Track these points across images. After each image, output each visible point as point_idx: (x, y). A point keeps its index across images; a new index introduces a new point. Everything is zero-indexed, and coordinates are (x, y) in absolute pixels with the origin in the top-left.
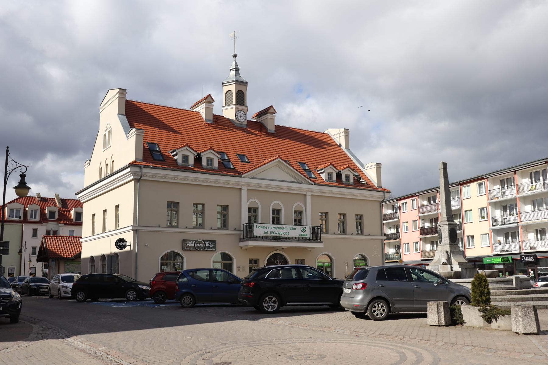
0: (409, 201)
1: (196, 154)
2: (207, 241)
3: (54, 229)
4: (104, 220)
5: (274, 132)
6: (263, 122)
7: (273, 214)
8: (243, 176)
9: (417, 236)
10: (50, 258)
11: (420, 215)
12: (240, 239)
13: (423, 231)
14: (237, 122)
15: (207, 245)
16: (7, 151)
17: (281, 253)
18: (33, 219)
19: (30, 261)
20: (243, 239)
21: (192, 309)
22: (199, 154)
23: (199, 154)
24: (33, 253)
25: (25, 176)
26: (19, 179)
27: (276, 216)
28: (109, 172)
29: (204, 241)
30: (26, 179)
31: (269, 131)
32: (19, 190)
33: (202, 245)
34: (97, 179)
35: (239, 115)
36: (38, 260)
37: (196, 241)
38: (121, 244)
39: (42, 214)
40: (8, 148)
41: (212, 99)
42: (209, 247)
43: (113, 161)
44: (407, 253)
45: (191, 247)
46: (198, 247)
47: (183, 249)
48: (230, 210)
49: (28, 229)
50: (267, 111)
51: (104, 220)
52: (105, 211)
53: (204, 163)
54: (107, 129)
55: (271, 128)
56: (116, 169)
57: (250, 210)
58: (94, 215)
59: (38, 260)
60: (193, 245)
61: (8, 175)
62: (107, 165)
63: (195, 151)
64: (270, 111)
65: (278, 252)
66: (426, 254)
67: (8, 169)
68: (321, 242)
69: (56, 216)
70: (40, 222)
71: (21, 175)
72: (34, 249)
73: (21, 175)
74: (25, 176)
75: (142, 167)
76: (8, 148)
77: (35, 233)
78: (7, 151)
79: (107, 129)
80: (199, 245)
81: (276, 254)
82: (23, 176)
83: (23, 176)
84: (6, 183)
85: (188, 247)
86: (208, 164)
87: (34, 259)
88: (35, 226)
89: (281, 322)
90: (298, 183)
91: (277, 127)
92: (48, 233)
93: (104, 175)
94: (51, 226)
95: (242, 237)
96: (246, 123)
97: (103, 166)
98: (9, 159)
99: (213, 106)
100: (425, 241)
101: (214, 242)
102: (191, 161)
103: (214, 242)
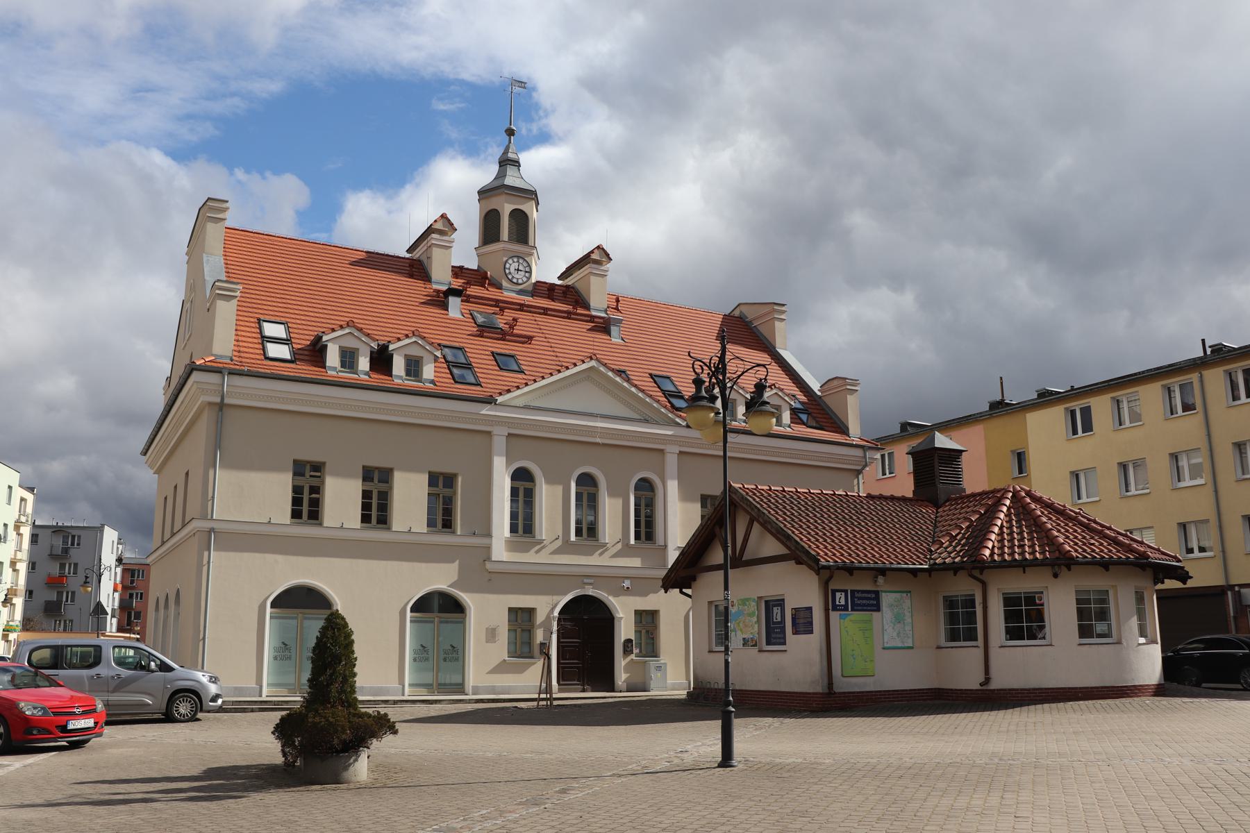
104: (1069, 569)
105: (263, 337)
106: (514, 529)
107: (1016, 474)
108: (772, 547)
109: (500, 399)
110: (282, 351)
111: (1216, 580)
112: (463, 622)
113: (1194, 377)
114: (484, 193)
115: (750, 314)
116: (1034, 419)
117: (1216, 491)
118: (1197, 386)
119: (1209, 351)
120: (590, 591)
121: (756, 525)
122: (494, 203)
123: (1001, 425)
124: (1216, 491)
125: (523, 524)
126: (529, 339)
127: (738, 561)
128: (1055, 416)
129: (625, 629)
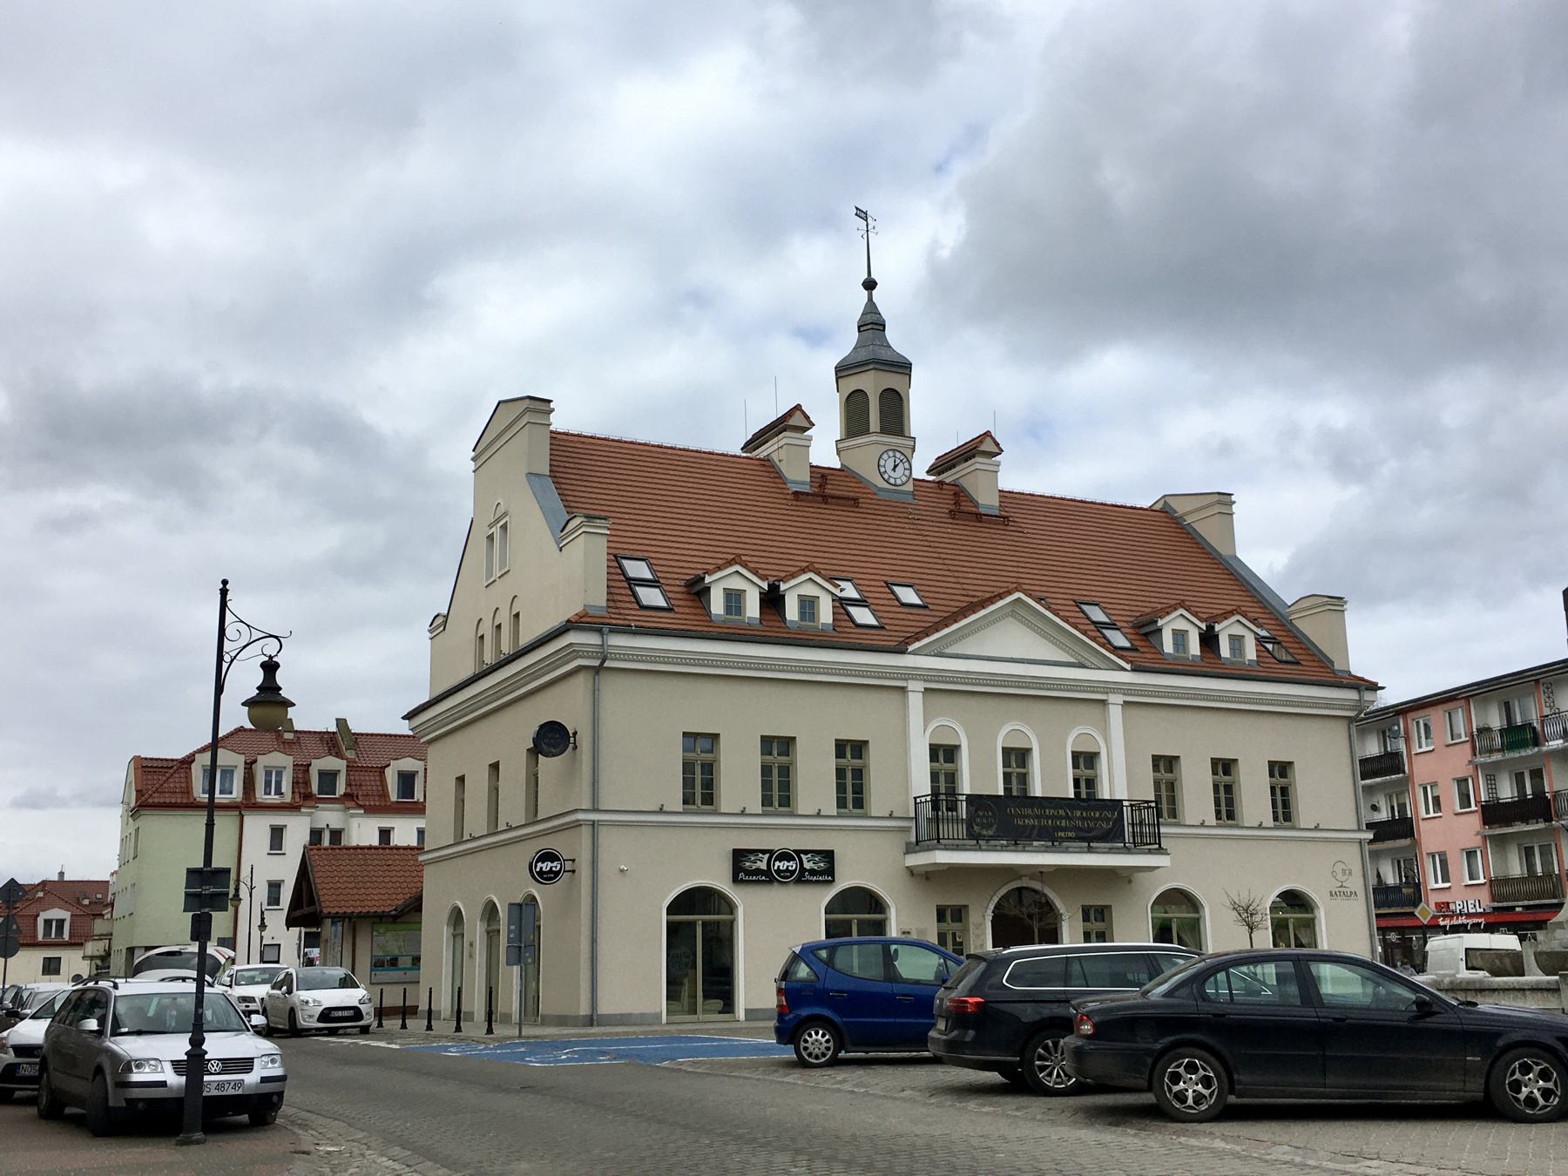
0: (1437, 716)
1: (765, 586)
2: (806, 852)
3: (335, 825)
4: (494, 792)
5: (997, 513)
6: (963, 482)
7: (1006, 764)
8: (911, 648)
9: (1465, 829)
10: (329, 916)
11: (1480, 759)
12: (908, 844)
13: (1493, 813)
14: (882, 484)
15: (807, 865)
16: (224, 592)
17: (1037, 886)
18: (273, 798)
19: (263, 926)
20: (917, 842)
21: (830, 1072)
22: (774, 588)
23: (774, 588)
24: (274, 899)
25: (277, 666)
26: (258, 677)
27: (1015, 770)
28: (506, 648)
29: (798, 852)
30: (280, 677)
31: (982, 511)
32: (259, 711)
33: (792, 865)
34: (468, 671)
35: (890, 464)
36: (290, 923)
37: (771, 852)
38: (546, 866)
39: (301, 782)
40: (225, 582)
41: (807, 418)
42: (812, 872)
43: (517, 616)
44: (1441, 885)
45: (758, 872)
46: (778, 871)
47: (736, 880)
48: (876, 761)
49: (257, 828)
50: (979, 449)
51: (494, 792)
52: (495, 767)
53: (792, 611)
54: (497, 521)
55: (797, 476)
56: (525, 639)
57: (935, 751)
58: (461, 780)
59: (290, 923)
60: (763, 866)
61: (225, 666)
62: (499, 627)
63: (763, 578)
64: (792, 422)
65: (1025, 883)
66: (1506, 890)
67: (227, 646)
68: (1161, 851)
69: (341, 788)
70: (292, 808)
71: (263, 665)
72: (275, 887)
73: (263, 665)
74: (277, 666)
75: (606, 630)
76: (225, 582)
77: (277, 834)
78: (224, 592)
79: (497, 521)
80: (783, 865)
81: (1020, 890)
82: (270, 667)
83: (270, 667)
84: (219, 689)
85: (749, 872)
86: (728, 610)
87: (277, 919)
88: (278, 819)
89: (1281, 1152)
90: (1082, 666)
91: (1005, 495)
92: (316, 834)
93: (489, 659)
94: (330, 817)
95: (913, 839)
96: (909, 487)
97: (487, 629)
98: (229, 617)
99: (810, 439)
100: (1500, 842)
101: (828, 856)
102: (752, 608)
103: (828, 856)
105: (629, 579)
115: (1180, 508)
122: (853, 383)
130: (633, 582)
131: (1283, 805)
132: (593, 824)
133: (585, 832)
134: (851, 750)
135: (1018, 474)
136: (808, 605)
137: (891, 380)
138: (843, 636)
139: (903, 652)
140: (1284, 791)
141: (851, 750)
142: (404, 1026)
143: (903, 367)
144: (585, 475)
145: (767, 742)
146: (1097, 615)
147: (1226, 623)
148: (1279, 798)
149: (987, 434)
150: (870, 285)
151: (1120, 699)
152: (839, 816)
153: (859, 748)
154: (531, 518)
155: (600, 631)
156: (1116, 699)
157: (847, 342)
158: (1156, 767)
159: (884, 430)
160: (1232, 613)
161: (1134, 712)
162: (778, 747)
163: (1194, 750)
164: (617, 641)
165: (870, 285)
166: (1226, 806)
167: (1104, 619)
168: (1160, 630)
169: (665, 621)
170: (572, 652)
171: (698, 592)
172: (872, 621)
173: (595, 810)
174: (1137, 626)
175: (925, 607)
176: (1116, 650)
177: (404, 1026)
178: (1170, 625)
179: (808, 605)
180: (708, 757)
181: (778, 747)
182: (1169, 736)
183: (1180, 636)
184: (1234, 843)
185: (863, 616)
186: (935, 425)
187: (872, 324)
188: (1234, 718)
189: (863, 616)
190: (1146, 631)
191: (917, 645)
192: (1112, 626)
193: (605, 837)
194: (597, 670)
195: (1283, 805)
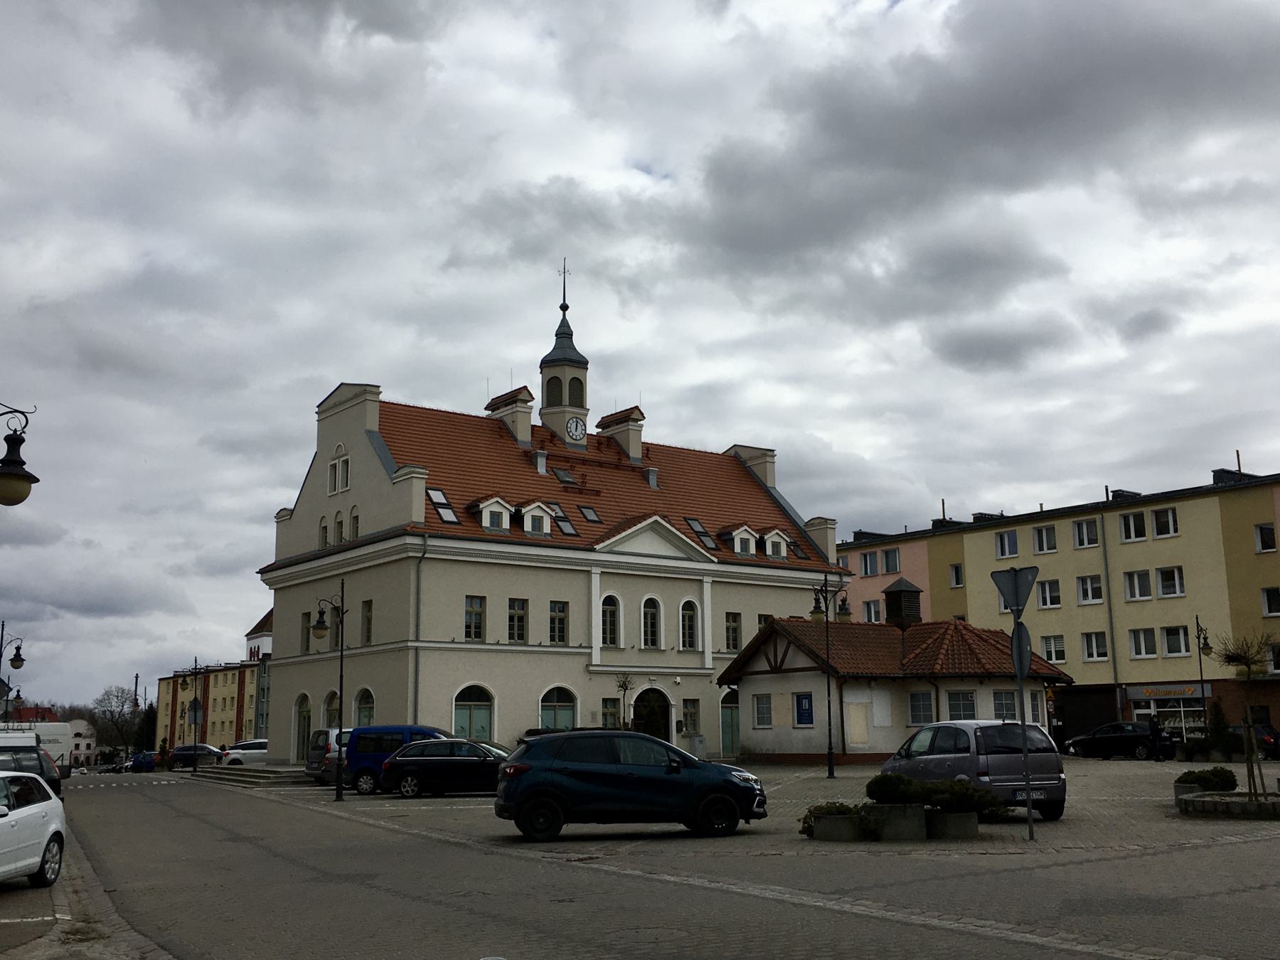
50: (631, 416)
53: (528, 526)
86: (492, 523)
96: (584, 442)
99: (641, 426)
104: (339, 798)
105: (434, 503)
106: (604, 642)
107: (954, 584)
108: (802, 661)
109: (597, 547)
110: (448, 515)
111: (1108, 680)
112: (490, 708)
113: (1097, 517)
114: (546, 363)
115: (744, 455)
116: (969, 540)
117: (1110, 610)
118: (1098, 524)
119: (1111, 495)
120: (657, 686)
121: (792, 647)
122: (555, 372)
123: (944, 543)
124: (1110, 610)
125: (611, 636)
126: (598, 493)
127: (777, 670)
128: (987, 539)
129: (675, 715)
130: (437, 505)
131: (559, 630)
132: (417, 649)
133: (411, 654)
134: (560, 607)
135: (654, 432)
136: (537, 521)
137: (575, 373)
138: (557, 540)
139: (593, 550)
140: (521, 619)
141: (560, 607)
142: (831, 775)
143: (582, 363)
144: (410, 435)
145: (512, 602)
146: (698, 528)
147: (487, 503)
148: (557, 625)
149: (637, 407)
150: (564, 307)
151: (599, 570)
152: (467, 642)
153: (524, 603)
154: (366, 463)
155: (422, 536)
156: (596, 570)
157: (547, 346)
158: (511, 607)
159: (571, 405)
160: (533, 501)
161: (717, 586)
162: (519, 608)
163: (499, 596)
164: (431, 542)
165: (564, 307)
166: (518, 627)
167: (700, 529)
168: (733, 539)
169: (457, 530)
170: (405, 548)
171: (473, 512)
172: (454, 519)
173: (417, 640)
174: (719, 536)
175: (600, 522)
176: (708, 549)
177: (831, 775)
178: (487, 509)
179: (537, 521)
180: (521, 612)
181: (519, 608)
182: (522, 586)
183: (745, 543)
184: (494, 655)
185: (567, 528)
186: (603, 398)
187: (564, 333)
188: (570, 575)
189: (448, 515)
190: (724, 539)
191: (602, 545)
192: (706, 534)
193: (423, 657)
194: (421, 559)
195: (559, 630)
